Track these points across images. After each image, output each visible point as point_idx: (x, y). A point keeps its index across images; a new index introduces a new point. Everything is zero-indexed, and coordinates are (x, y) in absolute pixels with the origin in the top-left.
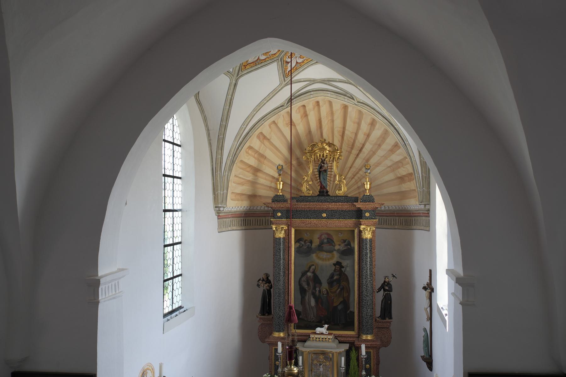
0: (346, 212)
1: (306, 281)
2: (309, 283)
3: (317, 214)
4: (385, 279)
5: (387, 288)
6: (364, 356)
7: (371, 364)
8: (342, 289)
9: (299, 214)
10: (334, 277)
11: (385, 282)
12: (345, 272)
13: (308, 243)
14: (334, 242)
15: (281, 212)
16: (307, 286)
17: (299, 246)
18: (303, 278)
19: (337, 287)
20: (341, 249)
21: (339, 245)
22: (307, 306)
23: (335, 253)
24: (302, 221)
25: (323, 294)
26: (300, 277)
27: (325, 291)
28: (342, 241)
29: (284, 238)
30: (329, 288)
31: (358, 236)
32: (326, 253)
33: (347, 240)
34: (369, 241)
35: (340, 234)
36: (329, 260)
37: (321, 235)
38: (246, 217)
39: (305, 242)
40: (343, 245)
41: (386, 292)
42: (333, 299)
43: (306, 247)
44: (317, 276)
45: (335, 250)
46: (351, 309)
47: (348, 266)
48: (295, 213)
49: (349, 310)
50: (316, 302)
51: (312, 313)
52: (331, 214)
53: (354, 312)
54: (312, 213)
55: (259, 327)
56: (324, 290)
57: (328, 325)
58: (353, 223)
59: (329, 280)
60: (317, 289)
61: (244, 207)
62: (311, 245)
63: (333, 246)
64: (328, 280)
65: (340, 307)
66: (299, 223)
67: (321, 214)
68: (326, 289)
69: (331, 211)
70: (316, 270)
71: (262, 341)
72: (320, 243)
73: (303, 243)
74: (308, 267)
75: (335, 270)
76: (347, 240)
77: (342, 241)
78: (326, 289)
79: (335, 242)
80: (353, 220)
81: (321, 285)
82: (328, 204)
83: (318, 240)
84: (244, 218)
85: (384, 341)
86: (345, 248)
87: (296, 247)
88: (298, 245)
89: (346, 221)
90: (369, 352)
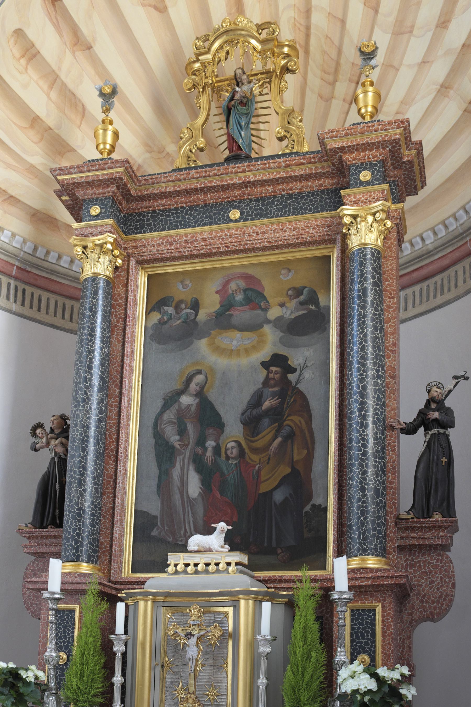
0: (303, 197)
1: (175, 421)
2: (186, 428)
3: (214, 214)
4: (429, 392)
5: (436, 415)
6: (341, 593)
7: (374, 652)
8: (290, 436)
9: (161, 221)
10: (262, 405)
11: (428, 402)
12: (297, 383)
13: (185, 308)
14: (265, 298)
15: (102, 204)
16: (178, 437)
17: (160, 320)
18: (168, 412)
19: (274, 431)
20: (287, 316)
21: (282, 305)
22: (177, 497)
23: (267, 329)
24: (166, 236)
25: (228, 458)
26: (159, 410)
27: (232, 448)
28: (290, 292)
29: (109, 282)
30: (245, 438)
31: (339, 263)
32: (238, 334)
33: (306, 287)
34: (373, 255)
35: (283, 272)
36: (247, 352)
37: (226, 284)
38: (26, 283)
39: (177, 307)
40: (293, 304)
41: (435, 431)
42: (259, 469)
43: (179, 322)
44: (211, 406)
45: (268, 322)
46: (317, 500)
47: (309, 365)
48: (148, 220)
49: (311, 503)
50: (202, 485)
51: (191, 520)
52: (256, 210)
53: (326, 508)
54: (198, 214)
55: (27, 569)
56: (230, 445)
57: (230, 528)
58: (323, 226)
59: (248, 412)
60: (210, 444)
61: (13, 235)
62: (196, 315)
63: (263, 310)
64: (243, 414)
65: (278, 497)
66: (159, 245)
67: (225, 212)
68: (235, 441)
69: (257, 200)
70: (206, 388)
71: (32, 612)
72: (221, 306)
73: (170, 310)
74: (184, 378)
75: (266, 383)
76: (305, 287)
77: (290, 292)
78: (235, 441)
79: (268, 298)
80: (320, 214)
81: (223, 433)
82: (244, 171)
83: (217, 298)
84: (21, 286)
85: (429, 598)
86: (301, 313)
87: (150, 325)
88: (156, 317)
89: (300, 221)
90: (369, 611)
